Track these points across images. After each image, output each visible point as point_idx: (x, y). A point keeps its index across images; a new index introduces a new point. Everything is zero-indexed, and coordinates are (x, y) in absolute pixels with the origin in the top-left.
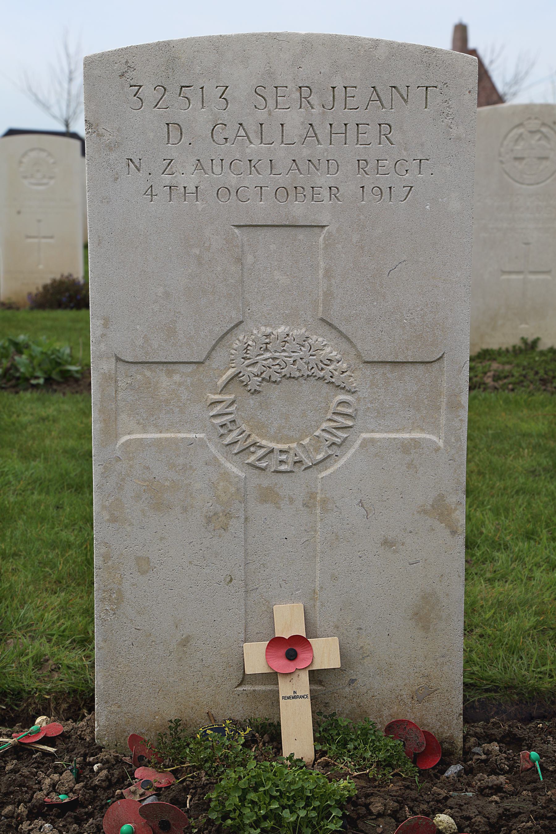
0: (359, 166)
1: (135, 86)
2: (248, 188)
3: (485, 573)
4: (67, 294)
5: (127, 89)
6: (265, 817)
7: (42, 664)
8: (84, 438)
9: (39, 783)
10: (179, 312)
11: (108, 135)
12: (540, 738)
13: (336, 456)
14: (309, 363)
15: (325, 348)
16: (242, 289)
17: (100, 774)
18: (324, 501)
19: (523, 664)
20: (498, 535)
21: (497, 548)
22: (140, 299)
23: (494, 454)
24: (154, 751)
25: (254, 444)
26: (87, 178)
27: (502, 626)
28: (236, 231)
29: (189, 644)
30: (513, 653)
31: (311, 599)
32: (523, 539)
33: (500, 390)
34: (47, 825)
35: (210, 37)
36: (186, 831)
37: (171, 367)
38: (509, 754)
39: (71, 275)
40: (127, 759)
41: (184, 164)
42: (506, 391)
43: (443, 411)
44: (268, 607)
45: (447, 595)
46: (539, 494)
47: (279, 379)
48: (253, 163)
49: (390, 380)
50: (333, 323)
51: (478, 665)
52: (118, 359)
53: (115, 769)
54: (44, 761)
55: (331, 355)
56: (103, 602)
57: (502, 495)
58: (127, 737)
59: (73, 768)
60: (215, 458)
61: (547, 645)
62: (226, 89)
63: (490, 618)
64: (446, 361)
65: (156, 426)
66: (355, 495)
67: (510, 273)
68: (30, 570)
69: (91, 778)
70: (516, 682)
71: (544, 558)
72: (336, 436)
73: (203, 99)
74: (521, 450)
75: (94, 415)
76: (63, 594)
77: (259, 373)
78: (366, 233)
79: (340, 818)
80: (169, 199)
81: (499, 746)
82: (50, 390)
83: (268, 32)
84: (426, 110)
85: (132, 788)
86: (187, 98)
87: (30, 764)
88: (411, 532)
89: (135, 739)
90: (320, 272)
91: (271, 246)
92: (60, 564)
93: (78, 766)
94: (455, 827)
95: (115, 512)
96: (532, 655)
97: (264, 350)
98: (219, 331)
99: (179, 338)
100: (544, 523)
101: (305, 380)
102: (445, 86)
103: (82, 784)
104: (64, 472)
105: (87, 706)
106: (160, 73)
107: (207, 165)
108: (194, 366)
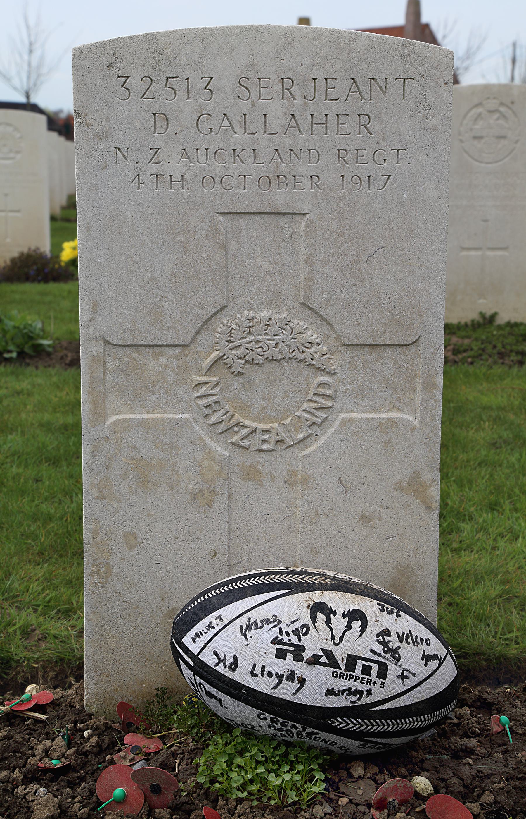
0: (339, 156)
1: (122, 77)
2: (232, 176)
3: (451, 544)
4: (35, 267)
5: (115, 80)
6: (251, 781)
7: (29, 634)
8: (59, 412)
9: (32, 748)
10: (166, 297)
12: (508, 703)
13: (316, 435)
15: (306, 331)
16: (226, 274)
17: (91, 740)
18: (305, 479)
19: (490, 631)
20: (463, 507)
21: (462, 519)
22: (127, 284)
23: (457, 426)
24: (142, 718)
25: (238, 424)
26: (76, 166)
27: (470, 595)
28: (221, 218)
30: (481, 621)
32: (486, 510)
33: (460, 364)
34: (42, 789)
35: (195, 29)
36: (176, 794)
37: (157, 350)
38: (480, 718)
39: (38, 249)
40: (117, 726)
41: (170, 153)
42: (466, 365)
43: (419, 392)
45: (422, 568)
46: (500, 465)
47: (262, 362)
48: (237, 152)
49: (368, 362)
50: (314, 307)
51: (448, 632)
53: (105, 735)
54: (36, 727)
55: (312, 338)
57: (465, 467)
58: (115, 704)
59: (65, 734)
60: (200, 438)
61: (512, 613)
62: (211, 80)
63: (457, 587)
64: (421, 344)
65: (143, 406)
66: (335, 472)
67: (469, 249)
68: (13, 542)
69: (81, 744)
70: (484, 649)
71: (508, 528)
72: (316, 416)
73: (188, 90)
76: (46, 565)
77: (243, 356)
78: (345, 221)
79: (323, 781)
81: (471, 711)
82: (23, 364)
83: (252, 24)
85: (122, 754)
86: (173, 88)
87: (22, 731)
88: (387, 508)
89: (123, 706)
90: (301, 258)
91: (254, 233)
92: (42, 536)
93: (69, 732)
94: (431, 788)
95: (104, 490)
96: (498, 623)
97: (247, 334)
99: (165, 321)
100: (506, 495)
101: (287, 362)
102: (422, 78)
103: (73, 750)
104: (41, 446)
105: (73, 674)
107: (192, 153)
108: (180, 349)
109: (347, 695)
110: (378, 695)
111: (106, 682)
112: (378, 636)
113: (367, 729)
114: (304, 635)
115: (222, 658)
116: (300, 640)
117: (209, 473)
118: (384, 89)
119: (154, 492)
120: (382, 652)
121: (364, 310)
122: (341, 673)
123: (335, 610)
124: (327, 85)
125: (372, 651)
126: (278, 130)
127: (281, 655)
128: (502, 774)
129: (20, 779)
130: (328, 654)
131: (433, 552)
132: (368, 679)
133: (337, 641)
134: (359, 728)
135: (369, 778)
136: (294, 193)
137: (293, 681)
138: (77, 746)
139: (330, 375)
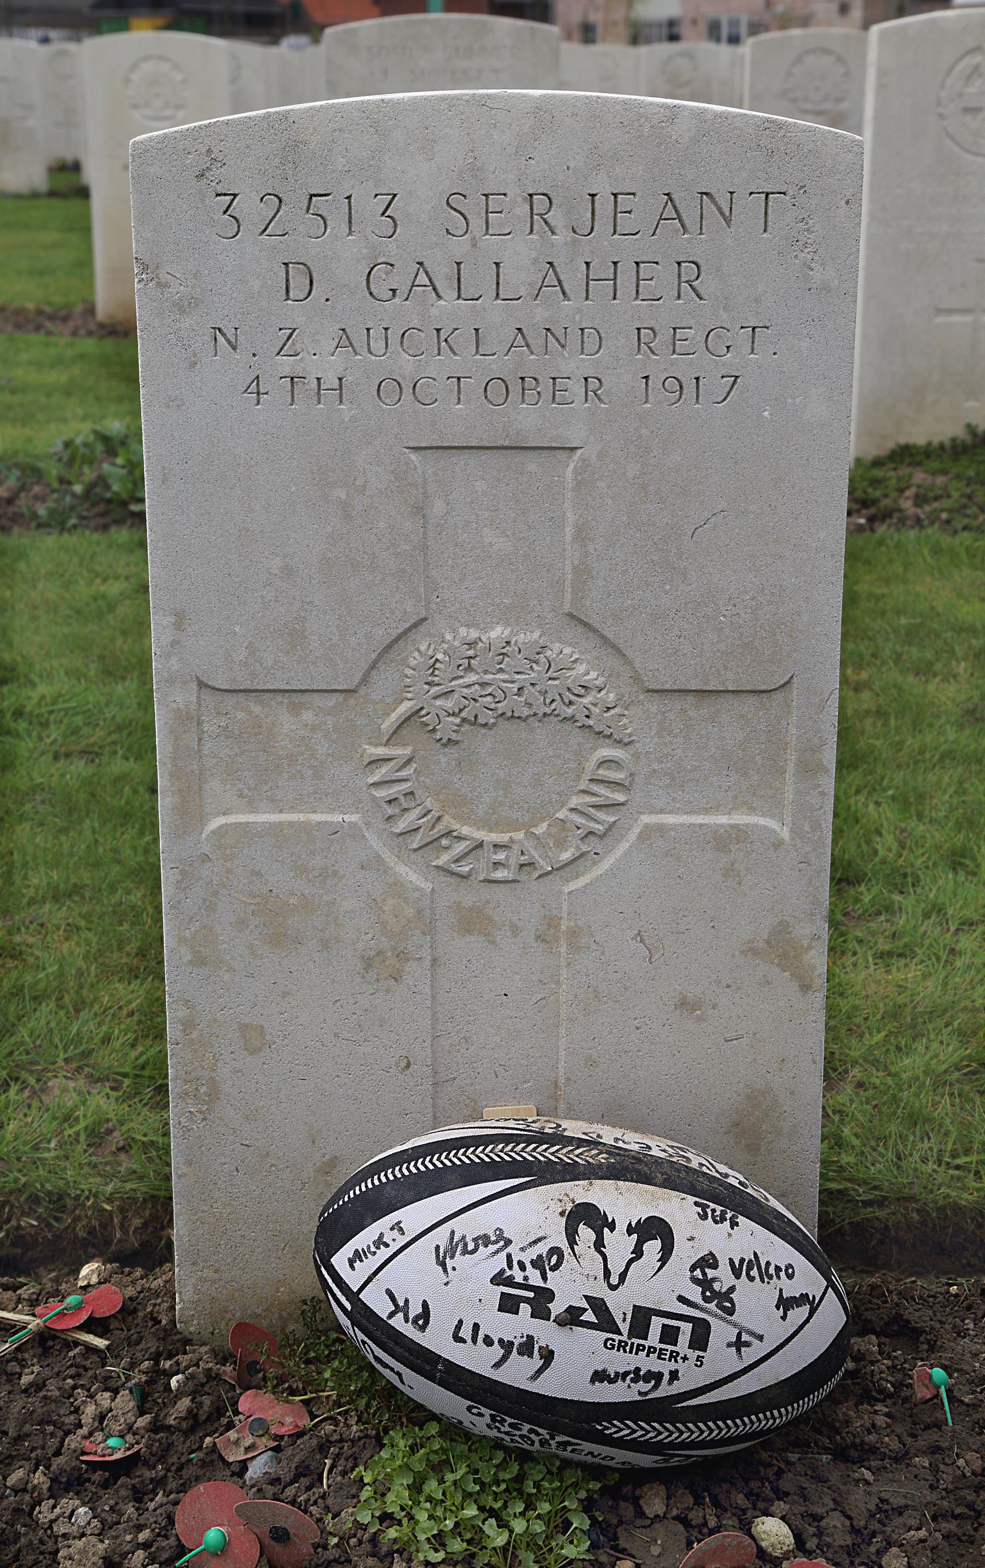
1: (225, 195)
2: (434, 379)
9: (77, 1411)
10: (311, 602)
11: (178, 286)
13: (595, 854)
14: (546, 692)
15: (577, 665)
16: (424, 561)
18: (573, 933)
22: (239, 579)
25: (448, 834)
28: (413, 457)
29: (336, 1170)
31: (550, 1097)
34: (82, 1510)
37: (297, 698)
44: (474, 1110)
45: (792, 1093)
47: (492, 721)
48: (443, 335)
50: (591, 622)
52: (202, 685)
56: (184, 1099)
60: (379, 858)
62: (393, 198)
67: (950, 312)
70: (917, 1190)
72: (595, 820)
74: (954, 663)
75: (162, 782)
77: (457, 710)
80: (289, 399)
84: (765, 235)
85: (232, 1435)
86: (320, 216)
88: (728, 986)
90: (567, 530)
91: (478, 484)
95: (202, 949)
97: (465, 670)
98: (383, 636)
99: (311, 647)
102: (801, 192)
103: (148, 1418)
106: (270, 170)
107: (359, 338)
108: (340, 697)
109: (632, 1380)
110: (691, 1378)
111: (214, 1282)
112: (693, 1268)
113: (670, 1439)
114: (553, 1269)
115: (401, 1304)
116: (544, 1278)
117: (395, 920)
118: (727, 214)
119: (293, 954)
120: (698, 1300)
121: (686, 627)
122: (620, 1341)
123: (613, 1220)
124: (616, 206)
125: (681, 1299)
126: (522, 292)
127: (508, 1305)
128: (926, 1506)
129: (45, 1487)
130: (597, 1305)
131: (813, 1066)
132: (672, 1352)
133: (614, 1280)
134: (656, 1437)
135: (675, 1518)
136: (553, 409)
137: (531, 1355)
138: (156, 1409)
139: (621, 745)
